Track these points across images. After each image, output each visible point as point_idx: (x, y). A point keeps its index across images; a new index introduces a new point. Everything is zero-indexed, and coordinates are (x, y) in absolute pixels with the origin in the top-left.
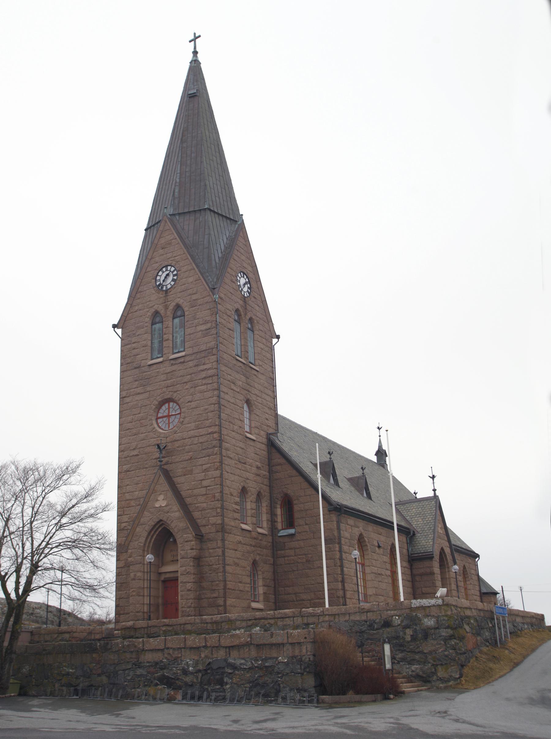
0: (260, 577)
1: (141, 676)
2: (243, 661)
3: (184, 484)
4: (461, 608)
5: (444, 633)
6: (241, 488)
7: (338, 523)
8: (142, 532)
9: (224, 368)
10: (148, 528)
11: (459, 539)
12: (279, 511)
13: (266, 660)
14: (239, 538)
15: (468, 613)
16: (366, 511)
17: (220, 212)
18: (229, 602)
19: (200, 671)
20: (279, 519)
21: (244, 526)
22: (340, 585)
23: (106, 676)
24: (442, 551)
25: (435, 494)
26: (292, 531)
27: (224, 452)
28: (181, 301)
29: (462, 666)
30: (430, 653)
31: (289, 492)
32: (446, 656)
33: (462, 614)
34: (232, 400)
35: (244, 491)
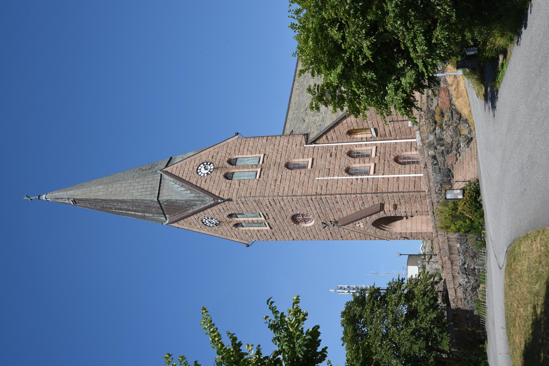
0: (405, 153)
3: (348, 212)
5: (438, 131)
8: (379, 232)
10: (378, 230)
19: (467, 277)
20: (364, 136)
28: (225, 216)
30: (452, 138)
35: (348, 171)
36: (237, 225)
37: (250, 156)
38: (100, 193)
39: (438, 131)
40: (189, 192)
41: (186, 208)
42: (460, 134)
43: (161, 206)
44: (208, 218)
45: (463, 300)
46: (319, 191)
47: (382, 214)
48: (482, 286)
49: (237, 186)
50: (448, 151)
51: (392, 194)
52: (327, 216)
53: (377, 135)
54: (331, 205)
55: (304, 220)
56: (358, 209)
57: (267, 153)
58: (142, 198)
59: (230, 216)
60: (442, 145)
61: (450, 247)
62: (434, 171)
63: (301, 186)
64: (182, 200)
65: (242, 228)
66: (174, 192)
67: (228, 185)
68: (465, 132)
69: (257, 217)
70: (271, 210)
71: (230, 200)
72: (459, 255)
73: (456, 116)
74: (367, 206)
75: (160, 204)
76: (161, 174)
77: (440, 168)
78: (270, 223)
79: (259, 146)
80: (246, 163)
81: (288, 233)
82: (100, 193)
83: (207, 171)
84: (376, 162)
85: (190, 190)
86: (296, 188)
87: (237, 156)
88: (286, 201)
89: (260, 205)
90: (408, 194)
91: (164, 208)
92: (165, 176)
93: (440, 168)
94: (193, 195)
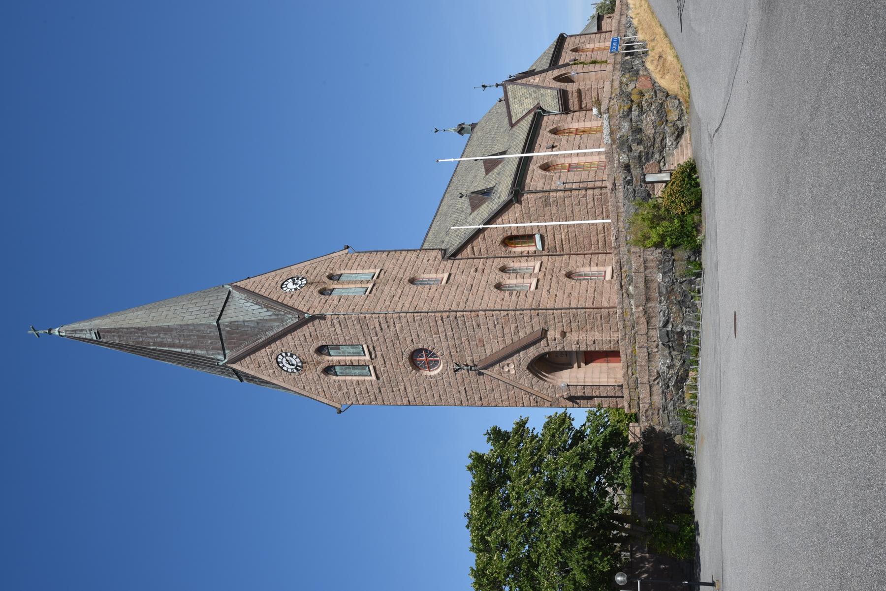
1: (674, 405)
2: (662, 314)
3: (494, 347)
4: (612, 93)
6: (495, 290)
7: (530, 192)
8: (537, 385)
9: (378, 307)
10: (536, 379)
11: (541, 58)
12: (518, 249)
13: (660, 293)
14: (545, 291)
15: (616, 84)
16: (515, 166)
17: (220, 309)
18: (606, 305)
19: (670, 353)
21: (533, 287)
22: (590, 192)
24: (558, 79)
25: (501, 85)
26: (537, 237)
27: (461, 308)
28: (312, 349)
29: (668, 95)
30: (655, 127)
31: (499, 239)
35: (499, 286)
36: (329, 370)
37: (361, 271)
38: (138, 320)
39: (635, 114)
40: (265, 310)
41: (257, 335)
42: (667, 121)
43: (220, 334)
44: (286, 354)
46: (454, 307)
47: (542, 348)
48: (692, 374)
49: (336, 302)
50: (648, 153)
51: (559, 311)
52: (462, 353)
53: (543, 249)
54: (470, 332)
55: (428, 363)
56: (508, 342)
57: (385, 268)
58: (197, 321)
59: (320, 350)
60: (640, 142)
61: (647, 281)
62: (626, 197)
63: (429, 301)
64: (252, 321)
65: (335, 378)
66: (242, 310)
68: (673, 116)
69: (358, 354)
70: (381, 340)
71: (322, 317)
72: (660, 302)
74: (522, 335)
75: (219, 329)
76: (230, 292)
77: (635, 191)
78: (377, 367)
79: (376, 261)
80: (354, 279)
81: (402, 388)
82: (138, 320)
83: (295, 286)
84: (541, 276)
85: (266, 307)
86: (421, 304)
87: (342, 272)
88: (404, 321)
89: (366, 330)
91: (224, 338)
92: (235, 293)
93: (635, 191)
94: (270, 313)
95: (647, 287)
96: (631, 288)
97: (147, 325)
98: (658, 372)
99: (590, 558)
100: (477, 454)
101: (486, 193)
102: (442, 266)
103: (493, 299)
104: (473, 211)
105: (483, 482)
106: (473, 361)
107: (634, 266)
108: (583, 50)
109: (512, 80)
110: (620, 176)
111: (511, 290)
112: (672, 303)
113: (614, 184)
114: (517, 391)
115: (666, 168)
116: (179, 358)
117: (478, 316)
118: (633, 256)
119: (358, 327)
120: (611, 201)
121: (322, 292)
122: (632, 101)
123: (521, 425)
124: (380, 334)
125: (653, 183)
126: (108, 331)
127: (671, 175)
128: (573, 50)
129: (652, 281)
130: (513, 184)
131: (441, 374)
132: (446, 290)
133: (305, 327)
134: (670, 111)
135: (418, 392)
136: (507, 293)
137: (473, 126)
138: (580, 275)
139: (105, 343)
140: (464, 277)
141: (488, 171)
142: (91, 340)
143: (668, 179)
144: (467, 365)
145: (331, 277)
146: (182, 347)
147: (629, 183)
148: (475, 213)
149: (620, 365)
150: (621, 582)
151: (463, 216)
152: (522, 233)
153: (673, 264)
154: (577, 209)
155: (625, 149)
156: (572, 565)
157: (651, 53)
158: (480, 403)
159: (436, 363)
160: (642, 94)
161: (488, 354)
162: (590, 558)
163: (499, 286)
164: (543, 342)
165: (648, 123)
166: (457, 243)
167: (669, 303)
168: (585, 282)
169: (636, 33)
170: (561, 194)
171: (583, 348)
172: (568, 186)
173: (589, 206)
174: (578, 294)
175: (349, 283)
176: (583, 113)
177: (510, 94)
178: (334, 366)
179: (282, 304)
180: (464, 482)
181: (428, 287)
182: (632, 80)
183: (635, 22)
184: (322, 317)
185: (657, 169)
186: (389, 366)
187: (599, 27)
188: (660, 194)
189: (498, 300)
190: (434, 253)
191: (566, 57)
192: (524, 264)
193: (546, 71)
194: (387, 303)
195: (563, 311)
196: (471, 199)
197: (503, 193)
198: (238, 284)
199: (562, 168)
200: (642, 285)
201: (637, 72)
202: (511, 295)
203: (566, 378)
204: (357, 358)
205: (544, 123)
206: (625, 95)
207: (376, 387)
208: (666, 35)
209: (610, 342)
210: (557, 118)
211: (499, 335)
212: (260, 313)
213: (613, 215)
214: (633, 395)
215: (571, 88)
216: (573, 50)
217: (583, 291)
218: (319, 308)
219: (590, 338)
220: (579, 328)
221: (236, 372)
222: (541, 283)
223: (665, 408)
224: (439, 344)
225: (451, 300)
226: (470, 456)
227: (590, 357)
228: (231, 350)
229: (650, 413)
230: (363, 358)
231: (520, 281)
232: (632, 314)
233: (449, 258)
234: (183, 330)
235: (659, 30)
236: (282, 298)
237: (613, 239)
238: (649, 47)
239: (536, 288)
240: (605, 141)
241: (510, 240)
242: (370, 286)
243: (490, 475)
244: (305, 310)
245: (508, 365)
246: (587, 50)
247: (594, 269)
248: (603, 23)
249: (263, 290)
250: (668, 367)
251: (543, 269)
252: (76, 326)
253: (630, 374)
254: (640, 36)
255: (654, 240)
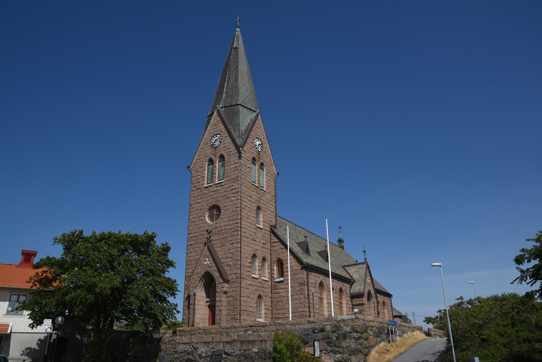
0: (263, 304)
1: (177, 358)
2: (233, 351)
3: (220, 252)
7: (307, 275)
8: (197, 277)
9: (244, 188)
10: (200, 276)
11: (379, 284)
12: (275, 268)
14: (251, 282)
15: (372, 324)
18: (242, 318)
19: (209, 356)
21: (253, 276)
22: (307, 309)
23: (448, 350)
24: (369, 292)
26: (282, 279)
27: (243, 234)
29: (366, 355)
30: (347, 347)
32: (357, 349)
33: (368, 324)
34: (249, 206)
35: (254, 256)
36: (211, 161)
38: (242, 66)
39: (355, 335)
41: (232, 124)
42: (351, 355)
45: (173, 350)
46: (243, 230)
47: (218, 280)
49: (248, 165)
50: (331, 343)
51: (239, 290)
54: (229, 239)
55: (213, 216)
56: (223, 261)
57: (266, 194)
58: (240, 94)
59: (222, 157)
60: (338, 338)
61: (253, 342)
62: (305, 329)
64: (239, 121)
65: (207, 164)
66: (245, 118)
67: (249, 159)
69: (219, 177)
70: (226, 190)
71: (240, 158)
72: (240, 350)
73: (366, 350)
74: (226, 268)
75: (235, 105)
77: (308, 335)
79: (270, 189)
81: (199, 201)
82: (242, 66)
85: (247, 129)
86: (245, 212)
87: (265, 170)
88: (236, 202)
89: (232, 181)
90: (239, 304)
93: (308, 335)
94: (243, 131)
95: (249, 342)
96: (250, 332)
97: (239, 71)
98: (197, 348)
99: (82, 302)
100: (155, 237)
101: (307, 251)
102: (267, 225)
103: (247, 252)
104: (297, 243)
105: (137, 240)
106: (213, 240)
107: (263, 334)
108: (384, 307)
109: (368, 267)
110: (317, 326)
111: (252, 263)
112: (239, 358)
113: (313, 322)
114: (195, 266)
115: (323, 354)
116: (222, 86)
117: (238, 243)
118: (269, 333)
119: (234, 177)
120: (303, 320)
121: (254, 159)
122: (362, 333)
123: (171, 264)
124: (230, 189)
125: (314, 346)
126: (237, 53)
127: (319, 358)
128: (384, 301)
129: (253, 345)
130: (312, 266)
131: (206, 222)
132: (253, 226)
133: (235, 149)
134: (357, 357)
135: (197, 210)
136: (250, 261)
137: (343, 247)
138: (260, 304)
139: (231, 51)
140: (260, 237)
141: (319, 253)
142: (233, 44)
143: (316, 356)
144: (210, 237)
145: (262, 164)
146: (227, 87)
147: (313, 331)
148: (296, 244)
149: (207, 325)
150: (58, 321)
151: (294, 238)
152: (285, 270)
153: (263, 359)
154: (298, 302)
155: (333, 329)
156: (79, 291)
157: (389, 345)
158: (189, 244)
159: (212, 220)
160: (367, 339)
161: (216, 249)
162: (82, 302)
163: (254, 256)
164: (221, 280)
165: (349, 343)
166: (280, 233)
167: (239, 356)
168: (255, 306)
169: (400, 336)
170: (306, 293)
171: (217, 304)
172: (311, 297)
173: (299, 309)
174: (248, 301)
175: (259, 173)
176: (351, 306)
177: (361, 266)
178: (213, 164)
179: (248, 137)
180: (137, 229)
181: (255, 216)
182: (374, 333)
183: (405, 335)
184: (240, 158)
185: (322, 349)
186: (212, 194)
187: (396, 317)
188: (306, 350)
189: (246, 255)
190: (274, 221)
191: (381, 298)
192: (267, 271)
193: (374, 286)
194: (247, 193)
195: (239, 293)
196: (304, 242)
197: (307, 260)
198: (260, 116)
199: (321, 294)
200: (251, 338)
201: (379, 337)
202: (249, 263)
203: (201, 295)
204: (217, 176)
205: (345, 284)
206: (366, 329)
207: (201, 186)
208: (401, 354)
209: (220, 320)
210: (348, 292)
211: (227, 255)
212: (243, 128)
213: (294, 322)
214: (187, 333)
215: (365, 300)
216: (384, 301)
217: (250, 304)
218: (245, 156)
219: (222, 308)
220: (229, 302)
221: (212, 114)
222: (256, 280)
223: (176, 352)
224: (223, 221)
225: (247, 228)
226: (153, 233)
227: (212, 308)
228: (224, 111)
229: (173, 343)
230: (217, 179)
231: (257, 268)
232: (234, 333)
233: (271, 229)
234: (236, 88)
235: (403, 350)
236: (251, 137)
237: (280, 321)
238: (393, 344)
239: (253, 278)
240: (338, 317)
241: (281, 264)
242: (257, 185)
243: (142, 244)
244: (244, 149)
245: (209, 260)
246: (384, 309)
247: (263, 312)
248: (398, 319)
249: (256, 128)
250: (200, 355)
251: (264, 282)
252: (240, 38)
253: (199, 331)
254: (398, 338)
255: (278, 347)
